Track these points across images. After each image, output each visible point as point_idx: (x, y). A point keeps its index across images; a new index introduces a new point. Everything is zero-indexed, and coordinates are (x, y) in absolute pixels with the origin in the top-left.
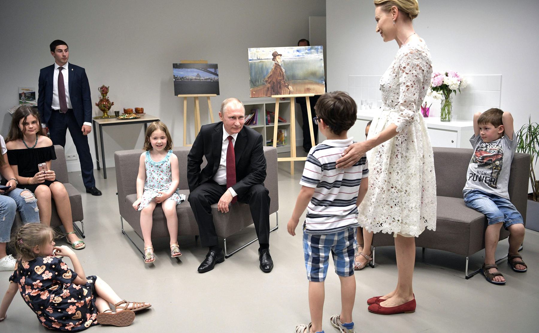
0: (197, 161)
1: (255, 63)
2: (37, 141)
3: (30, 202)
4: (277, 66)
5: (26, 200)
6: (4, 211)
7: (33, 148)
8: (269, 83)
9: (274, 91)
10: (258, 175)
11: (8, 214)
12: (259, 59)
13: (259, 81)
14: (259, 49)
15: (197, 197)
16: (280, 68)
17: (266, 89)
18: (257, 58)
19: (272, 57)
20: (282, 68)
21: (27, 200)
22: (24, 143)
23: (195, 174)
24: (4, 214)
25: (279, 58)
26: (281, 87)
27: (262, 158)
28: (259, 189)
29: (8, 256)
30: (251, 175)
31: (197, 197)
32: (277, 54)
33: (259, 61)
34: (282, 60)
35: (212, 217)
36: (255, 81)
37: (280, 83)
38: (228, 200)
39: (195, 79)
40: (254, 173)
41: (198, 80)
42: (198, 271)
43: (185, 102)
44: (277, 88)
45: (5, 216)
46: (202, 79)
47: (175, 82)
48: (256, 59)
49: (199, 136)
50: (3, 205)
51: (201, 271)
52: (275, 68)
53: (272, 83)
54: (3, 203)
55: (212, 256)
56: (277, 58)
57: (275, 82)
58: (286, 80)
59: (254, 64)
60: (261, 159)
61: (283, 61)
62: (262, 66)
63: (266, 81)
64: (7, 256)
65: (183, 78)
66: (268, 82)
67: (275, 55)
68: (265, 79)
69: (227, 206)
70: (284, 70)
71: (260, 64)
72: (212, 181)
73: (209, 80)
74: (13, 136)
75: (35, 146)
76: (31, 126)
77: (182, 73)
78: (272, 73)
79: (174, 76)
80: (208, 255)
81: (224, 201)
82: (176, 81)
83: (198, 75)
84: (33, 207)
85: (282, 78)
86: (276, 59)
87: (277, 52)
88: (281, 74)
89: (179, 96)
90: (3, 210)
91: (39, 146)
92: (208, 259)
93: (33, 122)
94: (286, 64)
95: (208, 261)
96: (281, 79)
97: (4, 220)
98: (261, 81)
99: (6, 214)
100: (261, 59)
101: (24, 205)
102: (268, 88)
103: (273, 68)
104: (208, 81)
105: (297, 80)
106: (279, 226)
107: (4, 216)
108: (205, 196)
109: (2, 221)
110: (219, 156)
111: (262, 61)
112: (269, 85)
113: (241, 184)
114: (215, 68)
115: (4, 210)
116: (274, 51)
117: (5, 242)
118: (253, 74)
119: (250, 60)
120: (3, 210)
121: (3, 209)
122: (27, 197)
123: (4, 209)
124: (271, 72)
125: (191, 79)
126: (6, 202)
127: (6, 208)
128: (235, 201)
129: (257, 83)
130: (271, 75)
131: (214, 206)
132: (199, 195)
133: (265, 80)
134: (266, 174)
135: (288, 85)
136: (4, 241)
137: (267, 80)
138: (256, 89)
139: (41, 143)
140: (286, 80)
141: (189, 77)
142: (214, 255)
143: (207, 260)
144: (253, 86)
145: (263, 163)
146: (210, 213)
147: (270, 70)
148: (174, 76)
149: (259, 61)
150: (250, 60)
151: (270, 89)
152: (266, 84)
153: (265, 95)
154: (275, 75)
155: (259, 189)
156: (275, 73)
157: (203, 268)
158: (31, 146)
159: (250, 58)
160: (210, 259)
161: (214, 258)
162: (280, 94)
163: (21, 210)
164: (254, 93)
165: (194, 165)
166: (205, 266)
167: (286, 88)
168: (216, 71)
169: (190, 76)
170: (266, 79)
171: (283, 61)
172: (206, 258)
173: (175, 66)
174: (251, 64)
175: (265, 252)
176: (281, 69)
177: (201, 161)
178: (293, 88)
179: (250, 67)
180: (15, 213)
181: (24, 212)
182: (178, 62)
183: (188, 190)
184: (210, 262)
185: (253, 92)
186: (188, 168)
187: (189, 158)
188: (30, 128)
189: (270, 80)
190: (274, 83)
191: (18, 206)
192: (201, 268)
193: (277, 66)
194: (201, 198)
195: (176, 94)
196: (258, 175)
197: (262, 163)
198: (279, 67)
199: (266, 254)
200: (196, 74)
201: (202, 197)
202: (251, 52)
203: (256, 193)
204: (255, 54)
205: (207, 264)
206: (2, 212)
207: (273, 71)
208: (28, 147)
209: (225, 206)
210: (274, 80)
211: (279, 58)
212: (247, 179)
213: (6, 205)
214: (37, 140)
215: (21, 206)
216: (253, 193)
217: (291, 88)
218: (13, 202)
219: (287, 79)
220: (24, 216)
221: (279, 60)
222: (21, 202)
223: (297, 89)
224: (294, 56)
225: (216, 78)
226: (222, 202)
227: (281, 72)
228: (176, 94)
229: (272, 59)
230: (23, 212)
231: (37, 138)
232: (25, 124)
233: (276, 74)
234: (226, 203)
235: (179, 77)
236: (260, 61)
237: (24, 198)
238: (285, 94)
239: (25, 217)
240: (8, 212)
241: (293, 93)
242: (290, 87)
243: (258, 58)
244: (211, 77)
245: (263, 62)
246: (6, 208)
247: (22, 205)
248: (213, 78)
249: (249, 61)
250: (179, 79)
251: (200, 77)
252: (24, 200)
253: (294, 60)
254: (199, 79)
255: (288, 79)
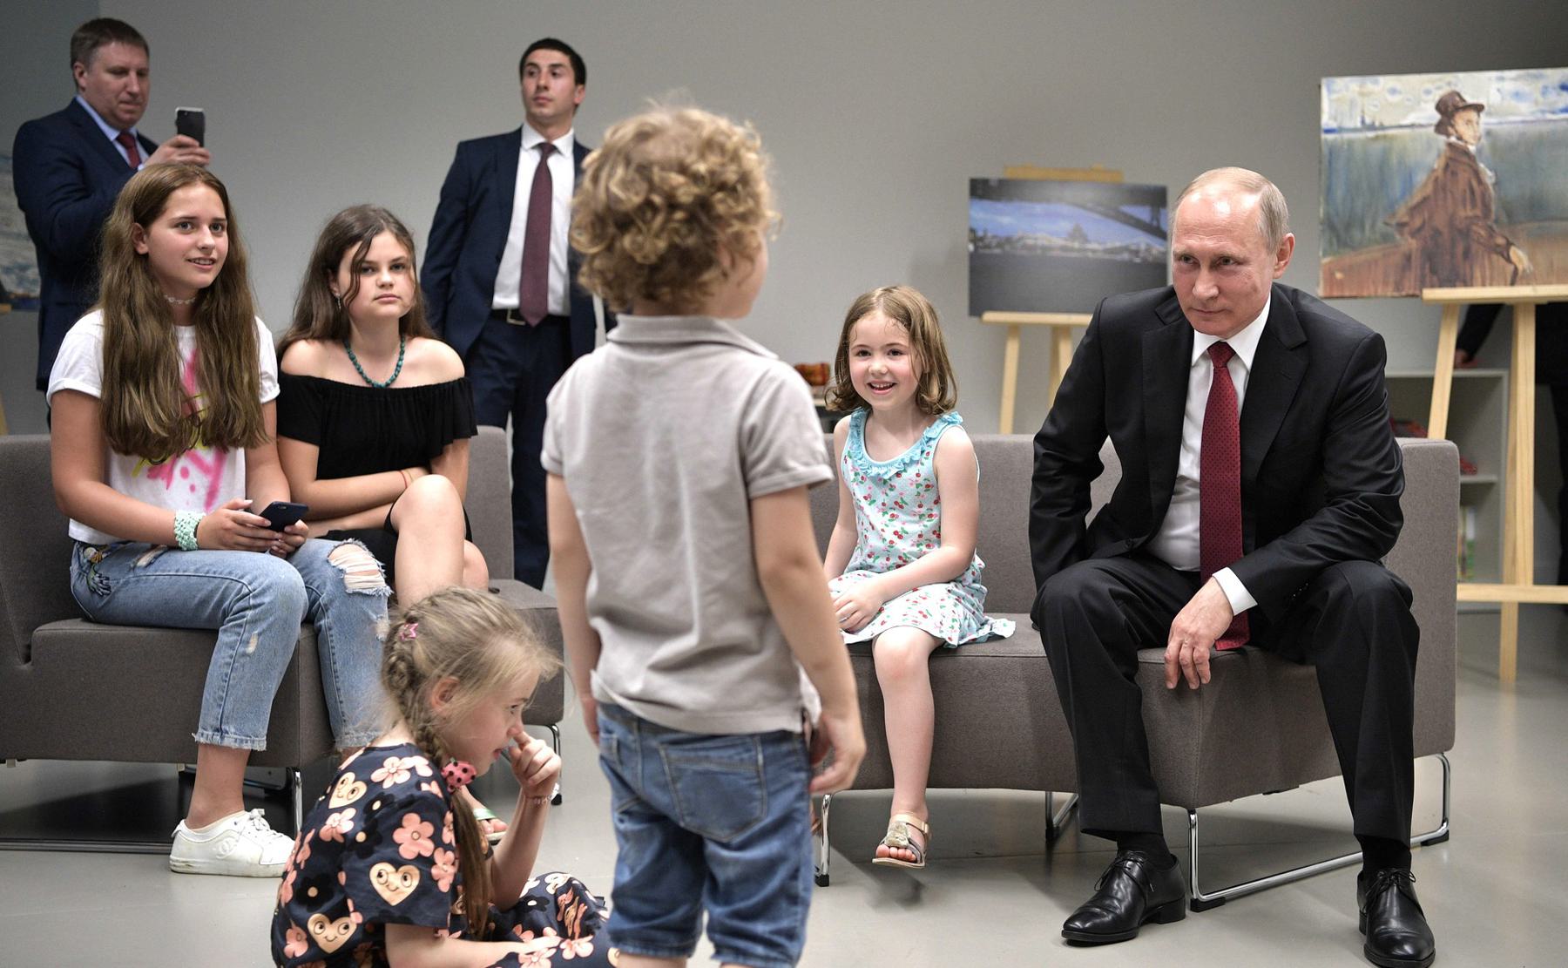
0: (1078, 459)
1: (1350, 143)
2: (400, 359)
3: (364, 592)
4: (1458, 156)
5: (349, 579)
6: (257, 610)
7: (388, 385)
8: (1413, 234)
9: (1433, 271)
10: (1359, 517)
11: (270, 627)
12: (1372, 127)
13: (1367, 227)
14: (1376, 83)
15: (1075, 593)
16: (1471, 167)
17: (1397, 259)
18: (1363, 122)
19: (1436, 117)
20: (1482, 166)
21: (354, 582)
22: (352, 359)
23: (1062, 519)
24: (254, 622)
25: (1469, 122)
26: (1473, 251)
27: (1378, 441)
28: (1362, 576)
29: (248, 815)
30: (1328, 516)
31: (1075, 593)
32: (1461, 104)
33: (1371, 134)
34: (1482, 128)
35: (1138, 697)
36: (1348, 226)
37: (1465, 233)
38: (1208, 626)
39: (1064, 248)
40: (1342, 505)
41: (1074, 255)
42: (1064, 934)
43: (1012, 349)
44: (1453, 255)
45: (259, 634)
46: (1094, 251)
47: (973, 257)
48: (1359, 125)
49: (1085, 343)
50: (255, 584)
51: (1076, 936)
52: (1447, 166)
53: (1426, 232)
54: (255, 578)
55: (1131, 878)
56: (1460, 122)
57: (1445, 231)
58: (1496, 221)
59: (1345, 147)
60: (1372, 447)
61: (1488, 133)
62: (1384, 163)
63: (1401, 225)
64: (243, 812)
65: (1009, 240)
66: (1406, 230)
67: (1449, 109)
68: (1394, 215)
69: (1203, 651)
70: (1489, 176)
71: (1377, 147)
72: (1148, 555)
73: (1126, 256)
74: (317, 325)
75: (393, 380)
76: (386, 276)
77: (1006, 220)
78: (1429, 190)
79: (972, 231)
80: (1116, 871)
81: (1192, 629)
82: (981, 251)
83: (1077, 234)
84: (370, 613)
85: (1478, 212)
86: (1453, 126)
87: (1459, 95)
88: (1476, 194)
89: (989, 316)
90: (255, 607)
91: (408, 380)
92: (1112, 889)
93: (396, 266)
94: (1502, 148)
95: (1112, 897)
96: (1477, 217)
97: (251, 649)
98: (1373, 226)
99: (264, 625)
100: (1382, 127)
101: (337, 603)
102: (1408, 258)
103: (1438, 164)
104: (1119, 257)
105: (1553, 219)
106: (1453, 826)
107: (256, 632)
108: (1116, 595)
109: (244, 655)
110: (1175, 441)
111: (1385, 137)
112: (1411, 244)
113: (1277, 556)
114: (1152, 205)
115: (260, 605)
116: (1445, 90)
117: (247, 747)
118: (1339, 193)
119: (1328, 131)
120: (255, 607)
121: (252, 602)
122: (356, 569)
123: (258, 601)
124: (1425, 185)
125: (1045, 248)
126: (267, 575)
127: (267, 599)
128: (1242, 628)
129: (1356, 234)
130: (1425, 199)
131: (1150, 656)
132: (1088, 589)
133: (1394, 222)
134: (1399, 517)
135: (1509, 244)
136: (242, 741)
137: (1406, 219)
138: (1349, 258)
139: (414, 367)
140: (1496, 221)
141: (1036, 239)
142: (1139, 875)
143: (1105, 892)
144: (1335, 247)
145: (1382, 467)
146: (1130, 677)
147: (1421, 178)
148: (972, 231)
149: (1371, 134)
150: (1328, 131)
151: (1416, 262)
152: (1398, 237)
153: (1391, 289)
154: (1445, 199)
155: (1362, 576)
156: (1444, 189)
157: (1087, 925)
158: (381, 377)
159: (1326, 120)
160: (1123, 889)
161: (1140, 886)
162: (1467, 283)
163: (322, 622)
164: (1339, 275)
165: (1057, 478)
166: (1096, 915)
167: (1495, 257)
168: (1156, 216)
169: (1039, 235)
170: (1402, 214)
171: (1488, 133)
172: (1098, 888)
173: (981, 189)
174: (1333, 150)
175: (1390, 885)
176: (1477, 173)
177: (1098, 468)
178: (1531, 259)
179: (1325, 161)
180: (297, 631)
181: (332, 632)
182: (993, 173)
183: (1024, 615)
184: (1119, 901)
185: (1332, 274)
186: (1036, 491)
187: (1038, 445)
188: (383, 286)
189: (1418, 222)
190: (1437, 232)
191: (313, 602)
192: (1078, 924)
193: (1458, 156)
194: (1094, 603)
195: (976, 309)
196: (1359, 517)
197: (1379, 463)
198: (1465, 159)
199: (1399, 891)
200: (1066, 226)
201: (1095, 593)
202: (1334, 96)
203: (1346, 592)
204: (1352, 103)
205: (1107, 909)
206: (249, 613)
207: (1436, 180)
208: (365, 379)
209: (1196, 654)
210: (1440, 221)
211: (1469, 122)
212: (1307, 535)
213: (269, 587)
214: (402, 353)
215: (325, 605)
216: (1334, 590)
217: (1520, 260)
218: (295, 579)
219: (1504, 219)
220: (332, 651)
221: (1470, 131)
222: (327, 588)
223: (1552, 264)
224: (1543, 112)
225: (1157, 246)
226: (1184, 632)
227: (1475, 183)
228: (976, 309)
229: (1432, 130)
230: (330, 629)
231: (402, 347)
232: (363, 267)
233: (1449, 195)
234: (1200, 637)
235: (994, 237)
236: (1377, 138)
237: (341, 571)
238: (1491, 285)
239: (333, 654)
240: (271, 619)
241: (1528, 279)
242: (1519, 255)
243: (1368, 121)
244: (1135, 241)
245: (1393, 138)
246: (267, 599)
247: (331, 601)
248: (1143, 247)
249: (1324, 136)
250: (994, 244)
251: (1086, 240)
252: (343, 579)
253: (1545, 128)
254: (1079, 250)
255: (1509, 214)
